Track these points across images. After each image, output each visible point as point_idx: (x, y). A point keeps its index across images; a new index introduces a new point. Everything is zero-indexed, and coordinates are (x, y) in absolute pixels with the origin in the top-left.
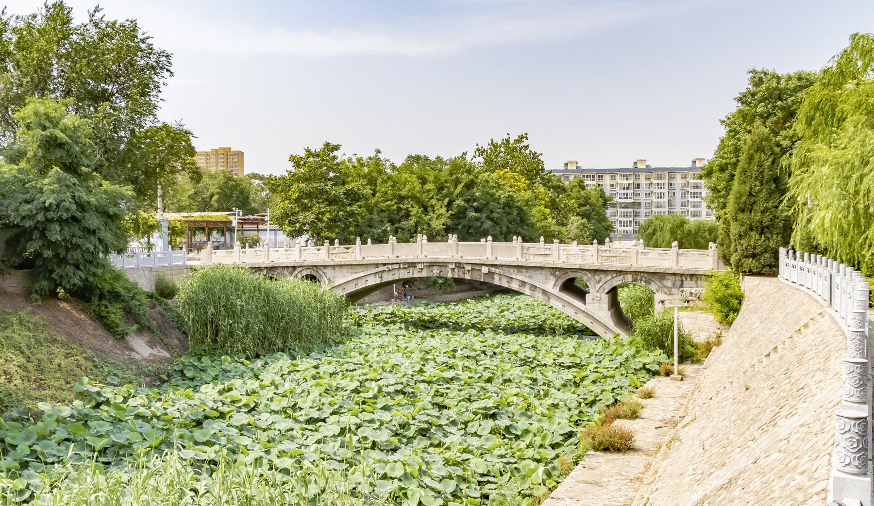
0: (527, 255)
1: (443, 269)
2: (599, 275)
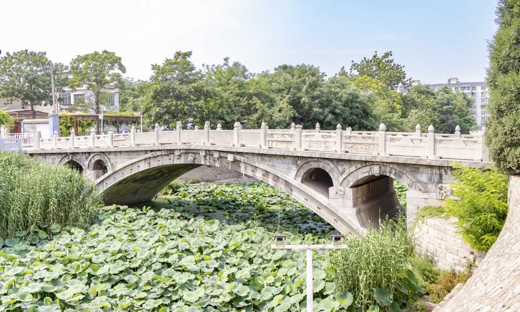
0: (270, 142)
1: (197, 156)
2: (342, 165)
